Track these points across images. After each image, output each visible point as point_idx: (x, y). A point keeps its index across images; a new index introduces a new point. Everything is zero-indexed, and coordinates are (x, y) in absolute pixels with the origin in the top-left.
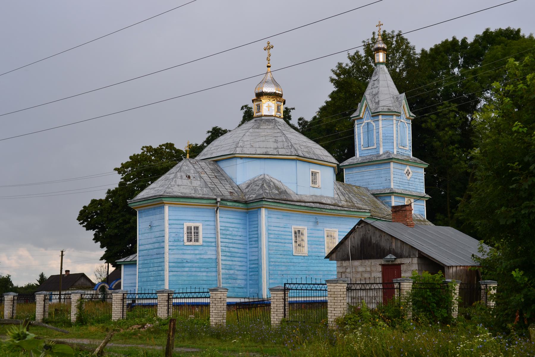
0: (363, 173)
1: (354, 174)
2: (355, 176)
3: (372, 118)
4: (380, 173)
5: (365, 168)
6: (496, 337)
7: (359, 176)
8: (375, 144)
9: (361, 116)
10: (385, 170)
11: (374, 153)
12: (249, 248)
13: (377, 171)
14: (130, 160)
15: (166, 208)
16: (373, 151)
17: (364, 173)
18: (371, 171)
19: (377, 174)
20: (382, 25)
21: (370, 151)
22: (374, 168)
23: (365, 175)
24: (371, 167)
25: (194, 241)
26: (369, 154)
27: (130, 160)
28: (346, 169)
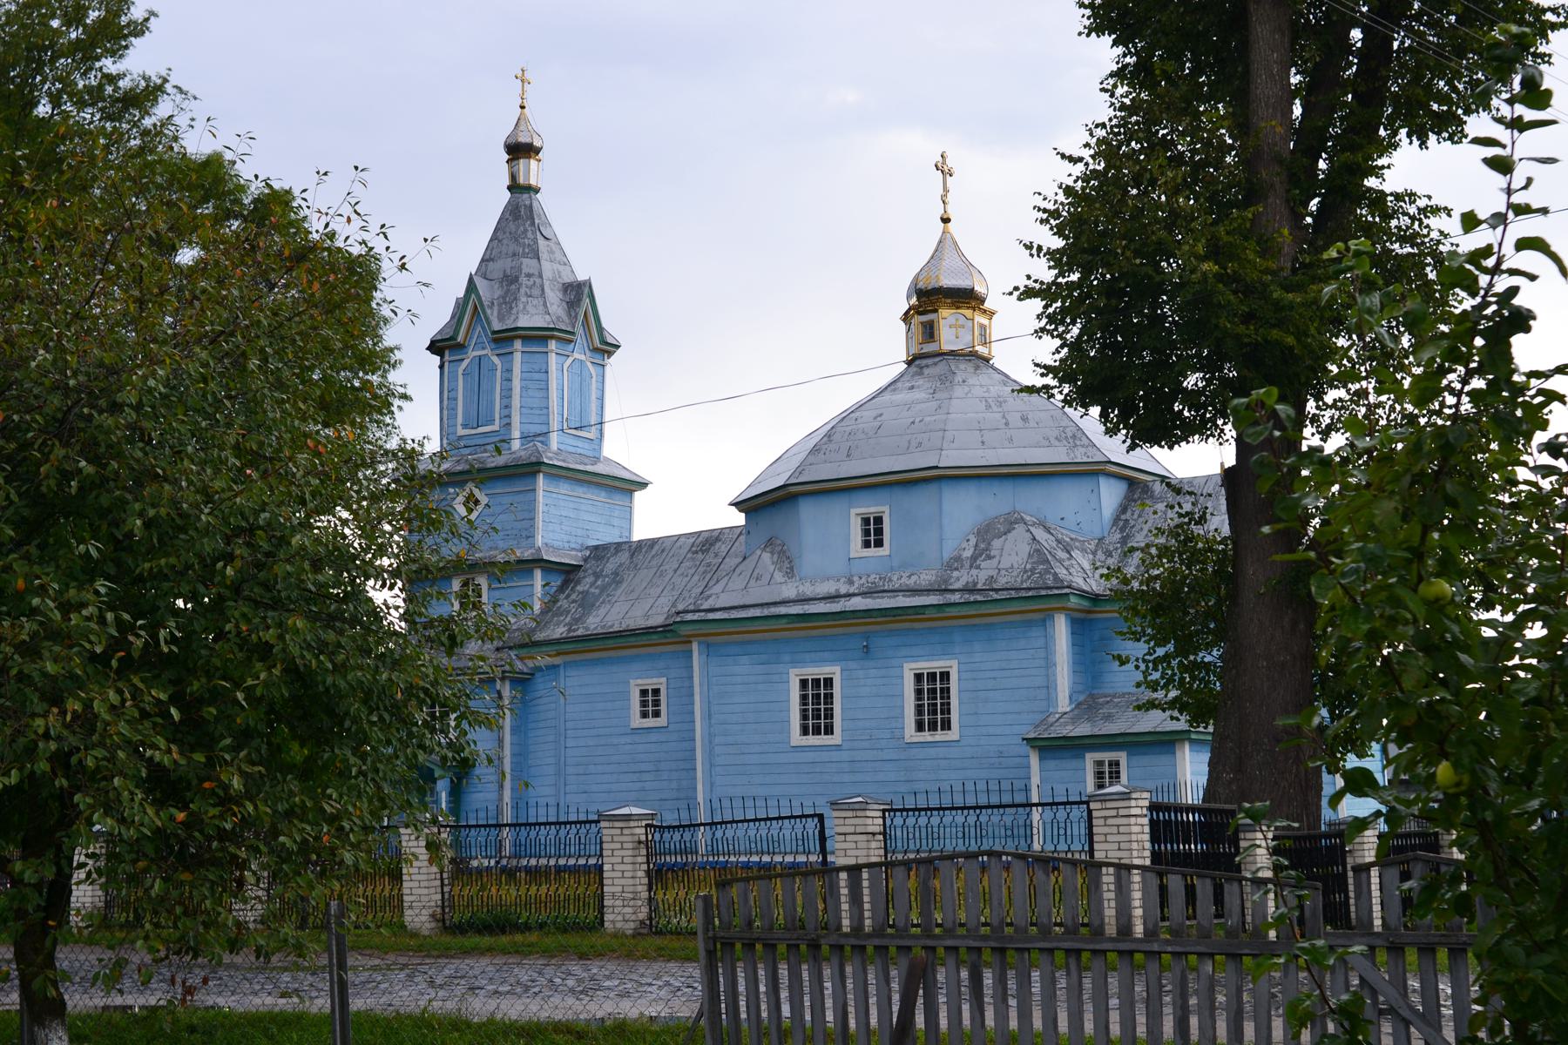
2: (562, 503)
7: (571, 505)
21: (579, 443)
26: (579, 451)
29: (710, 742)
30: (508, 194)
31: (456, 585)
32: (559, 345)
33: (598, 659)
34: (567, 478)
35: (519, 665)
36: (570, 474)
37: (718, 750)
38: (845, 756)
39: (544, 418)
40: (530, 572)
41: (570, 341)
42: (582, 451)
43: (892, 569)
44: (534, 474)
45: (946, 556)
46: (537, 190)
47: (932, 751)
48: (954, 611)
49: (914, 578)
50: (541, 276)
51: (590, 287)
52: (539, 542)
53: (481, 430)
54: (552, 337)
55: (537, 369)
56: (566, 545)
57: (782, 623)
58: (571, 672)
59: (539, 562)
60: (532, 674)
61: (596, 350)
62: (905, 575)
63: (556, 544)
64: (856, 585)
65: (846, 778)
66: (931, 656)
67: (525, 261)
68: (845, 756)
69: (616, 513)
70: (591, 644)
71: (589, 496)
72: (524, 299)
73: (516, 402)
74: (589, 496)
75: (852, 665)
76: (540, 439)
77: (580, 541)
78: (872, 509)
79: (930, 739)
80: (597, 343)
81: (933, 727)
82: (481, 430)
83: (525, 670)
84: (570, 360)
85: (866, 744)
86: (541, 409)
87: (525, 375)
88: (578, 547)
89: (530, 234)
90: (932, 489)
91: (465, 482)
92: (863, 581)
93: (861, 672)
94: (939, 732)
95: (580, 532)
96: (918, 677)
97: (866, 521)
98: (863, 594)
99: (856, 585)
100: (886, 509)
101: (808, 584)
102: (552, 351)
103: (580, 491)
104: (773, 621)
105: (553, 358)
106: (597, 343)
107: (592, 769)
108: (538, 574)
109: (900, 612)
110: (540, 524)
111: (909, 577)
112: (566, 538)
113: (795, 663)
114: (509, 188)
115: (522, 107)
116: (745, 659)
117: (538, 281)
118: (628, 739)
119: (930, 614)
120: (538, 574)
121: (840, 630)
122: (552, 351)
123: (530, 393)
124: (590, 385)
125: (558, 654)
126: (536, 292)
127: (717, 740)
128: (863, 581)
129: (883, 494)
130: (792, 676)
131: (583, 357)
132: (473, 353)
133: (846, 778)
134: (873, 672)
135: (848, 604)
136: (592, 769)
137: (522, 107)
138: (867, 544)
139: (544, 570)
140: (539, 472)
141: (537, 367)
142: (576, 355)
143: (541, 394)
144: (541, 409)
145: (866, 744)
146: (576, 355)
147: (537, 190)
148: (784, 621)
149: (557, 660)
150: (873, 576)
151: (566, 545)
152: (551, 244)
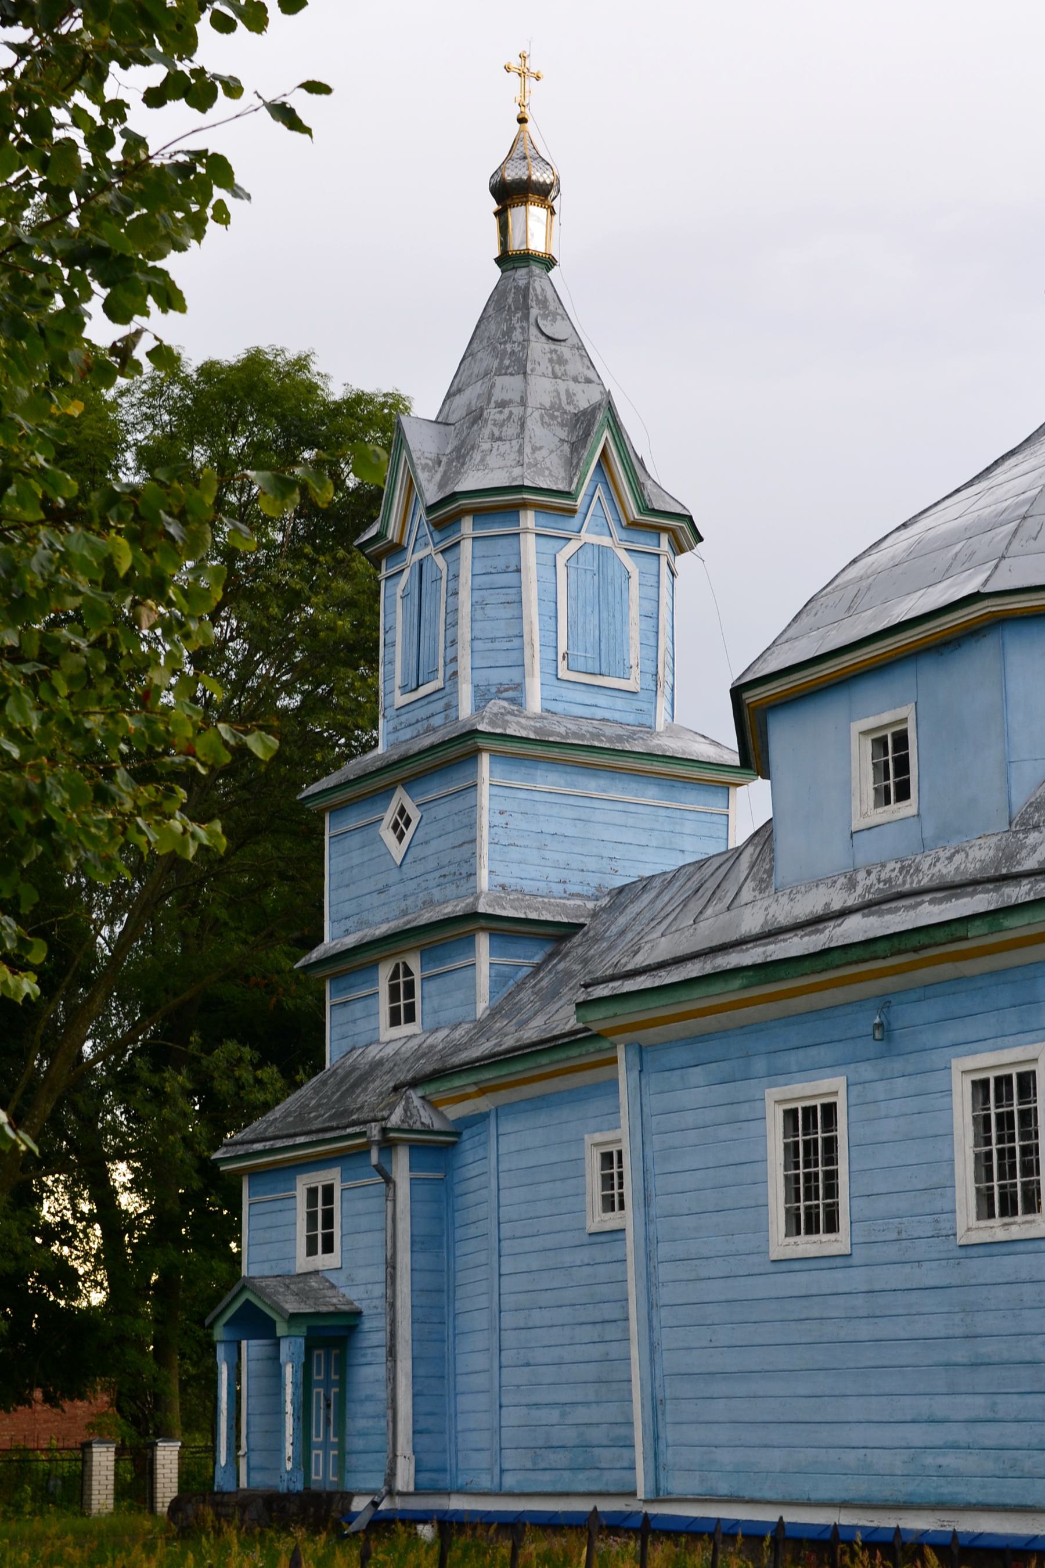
0: (587, 803)
1: (537, 796)
2: (541, 809)
3: (624, 535)
4: (678, 829)
5: (602, 782)
6: (62, 1261)
7: (570, 813)
8: (635, 673)
9: (392, 533)
10: (703, 817)
11: (620, 710)
12: (619, 1141)
13: (662, 812)
14: (172, 263)
15: (485, 759)
16: (620, 703)
17: (596, 804)
18: (632, 808)
19: (657, 826)
20: (538, 78)
21: (602, 700)
22: (650, 795)
23: (598, 816)
24: (634, 785)
25: (815, 1107)
26: (600, 713)
27: (172, 263)
28: (494, 754)
29: (648, 1256)
30: (496, 272)
31: (385, 972)
32: (543, 519)
33: (542, 1097)
34: (553, 761)
35: (426, 1117)
36: (554, 753)
37: (665, 1272)
38: (856, 1279)
39: (513, 656)
40: (469, 940)
41: (571, 512)
42: (607, 715)
43: (924, 847)
44: (473, 755)
45: (1020, 800)
46: (548, 262)
47: (1008, 1265)
48: (1018, 926)
49: (958, 858)
50: (523, 403)
51: (611, 407)
52: (484, 881)
53: (423, 691)
54: (525, 505)
55: (501, 567)
56: (558, 889)
57: (732, 991)
58: (506, 1127)
59: (473, 919)
60: (458, 1134)
61: (633, 526)
62: (944, 855)
63: (529, 886)
64: (859, 890)
65: (864, 1330)
66: (998, 1039)
67: (500, 381)
68: (856, 1279)
69: (688, 827)
70: (519, 1067)
71: (613, 795)
72: (485, 446)
73: (464, 632)
74: (613, 795)
75: (866, 1071)
76: (510, 694)
77: (594, 880)
78: (886, 718)
79: (1001, 1235)
80: (634, 514)
81: (1008, 1208)
82: (423, 691)
83: (438, 1125)
84: (572, 547)
85: (892, 1252)
86: (510, 638)
87: (479, 580)
88: (591, 891)
89: (517, 335)
90: (987, 646)
91: (387, 791)
92: (873, 877)
93: (880, 1086)
94: (1020, 1218)
95: (592, 864)
96: (980, 1086)
97: (880, 744)
98: (866, 907)
99: (859, 890)
100: (907, 711)
101: (784, 900)
102: (526, 531)
103: (592, 785)
104: (717, 987)
105: (529, 544)
106: (634, 514)
107: (538, 1317)
108: (483, 942)
109: (923, 939)
110: (484, 848)
111: (950, 859)
112: (554, 875)
113: (776, 1074)
114: (499, 261)
115: (522, 120)
116: (696, 1075)
117: (517, 411)
118: (583, 1255)
119: (979, 936)
120: (483, 942)
121: (838, 995)
122: (526, 531)
123: (490, 611)
124: (626, 590)
125: (482, 1092)
126: (511, 430)
127: (664, 1250)
128: (873, 877)
129: (902, 681)
130: (769, 1103)
131: (606, 541)
132: (412, 558)
133: (864, 1330)
134: (901, 1085)
135: (839, 931)
136: (538, 1317)
137: (522, 120)
138: (883, 797)
139: (493, 934)
140: (479, 751)
141: (500, 564)
142: (586, 537)
143: (510, 612)
144: (510, 638)
145: (892, 1252)
146: (586, 537)
147: (548, 262)
148: (737, 983)
149: (482, 1104)
150: (891, 865)
151: (558, 889)
152: (564, 350)
